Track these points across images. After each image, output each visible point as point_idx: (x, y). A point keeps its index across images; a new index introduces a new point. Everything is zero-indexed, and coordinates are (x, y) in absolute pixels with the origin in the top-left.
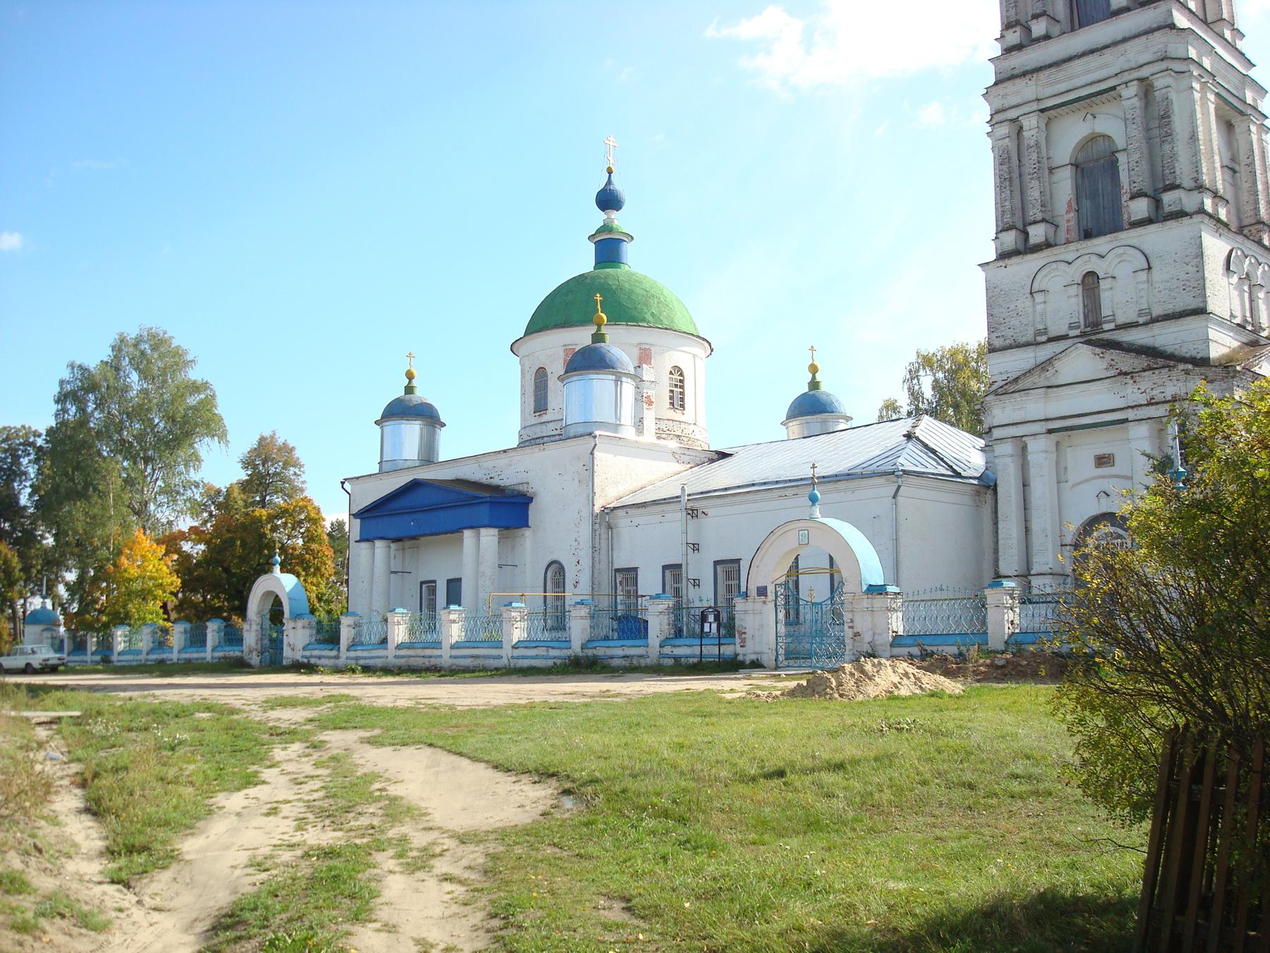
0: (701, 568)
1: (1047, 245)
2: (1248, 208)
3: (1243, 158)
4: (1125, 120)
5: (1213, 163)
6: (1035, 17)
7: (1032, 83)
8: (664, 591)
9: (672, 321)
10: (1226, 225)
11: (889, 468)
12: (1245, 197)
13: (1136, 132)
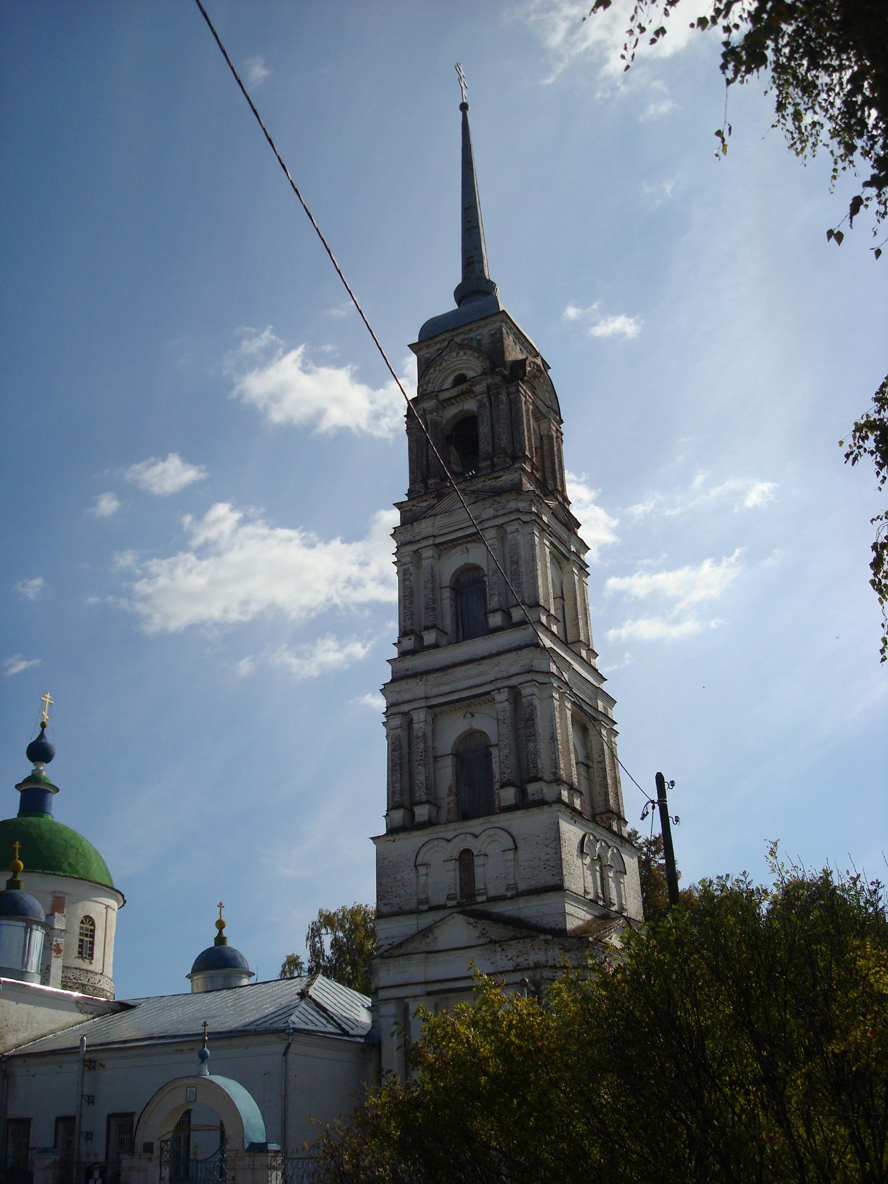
0: (95, 1122)
1: (430, 823)
2: (599, 799)
3: (595, 755)
4: (498, 720)
5: (570, 760)
6: (427, 628)
7: (422, 683)
8: (55, 1146)
9: (88, 872)
10: (580, 813)
11: (281, 1025)
12: (597, 789)
13: (506, 731)
